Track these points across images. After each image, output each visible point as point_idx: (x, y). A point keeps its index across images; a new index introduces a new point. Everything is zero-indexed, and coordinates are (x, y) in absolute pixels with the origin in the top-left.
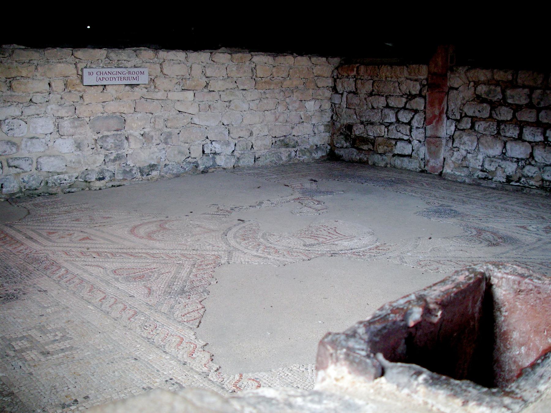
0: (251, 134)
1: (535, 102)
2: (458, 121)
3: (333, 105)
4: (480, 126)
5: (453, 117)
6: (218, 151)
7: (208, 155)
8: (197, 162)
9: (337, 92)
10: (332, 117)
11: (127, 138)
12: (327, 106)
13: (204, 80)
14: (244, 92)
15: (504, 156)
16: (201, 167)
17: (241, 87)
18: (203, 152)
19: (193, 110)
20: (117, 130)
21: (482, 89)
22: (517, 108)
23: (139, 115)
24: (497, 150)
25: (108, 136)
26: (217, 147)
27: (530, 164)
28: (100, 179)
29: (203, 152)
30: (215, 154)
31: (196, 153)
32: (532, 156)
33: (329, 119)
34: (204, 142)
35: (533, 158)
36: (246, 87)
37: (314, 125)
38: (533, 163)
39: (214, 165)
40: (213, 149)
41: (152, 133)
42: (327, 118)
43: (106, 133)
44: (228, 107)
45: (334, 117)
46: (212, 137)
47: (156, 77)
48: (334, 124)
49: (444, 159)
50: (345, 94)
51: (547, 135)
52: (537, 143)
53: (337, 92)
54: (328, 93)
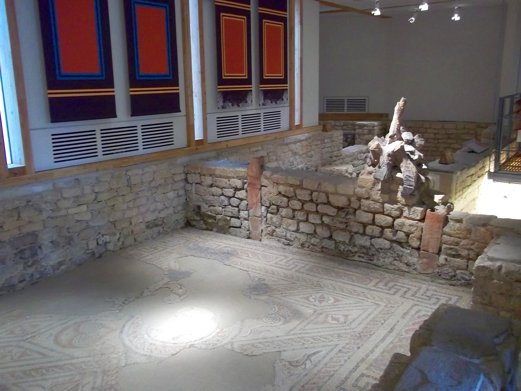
0: (131, 223)
1: (314, 199)
2: (268, 207)
3: (186, 191)
4: (284, 212)
5: (265, 205)
6: (108, 241)
7: (101, 245)
8: (93, 252)
9: (188, 183)
10: (186, 199)
11: (40, 247)
12: (182, 192)
13: (93, 196)
14: (123, 197)
15: (297, 231)
16: (97, 255)
17: (121, 194)
18: (98, 243)
19: (88, 217)
20: (32, 244)
21: (282, 188)
22: (303, 203)
23: (47, 230)
24: (293, 228)
25: (25, 249)
26: (107, 238)
27: (314, 237)
28: (21, 282)
29: (98, 243)
30: (106, 243)
31: (92, 245)
32: (315, 231)
33: (184, 201)
34: (97, 237)
35: (316, 233)
36: (124, 193)
37: (174, 207)
38: (316, 236)
39: (107, 250)
40: (105, 240)
41: (59, 240)
42: (182, 200)
43: (23, 247)
44: (113, 209)
45: (188, 199)
46: (103, 232)
47: (58, 200)
48: (188, 204)
49: (262, 231)
50: (194, 184)
51: (323, 220)
52: (318, 224)
53: (188, 183)
54: (182, 184)
